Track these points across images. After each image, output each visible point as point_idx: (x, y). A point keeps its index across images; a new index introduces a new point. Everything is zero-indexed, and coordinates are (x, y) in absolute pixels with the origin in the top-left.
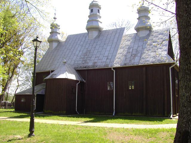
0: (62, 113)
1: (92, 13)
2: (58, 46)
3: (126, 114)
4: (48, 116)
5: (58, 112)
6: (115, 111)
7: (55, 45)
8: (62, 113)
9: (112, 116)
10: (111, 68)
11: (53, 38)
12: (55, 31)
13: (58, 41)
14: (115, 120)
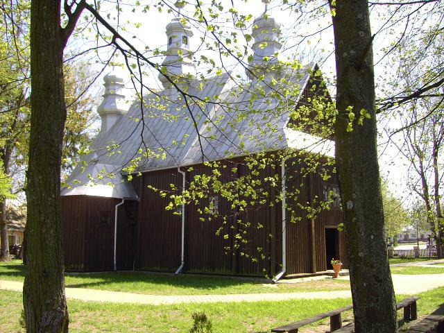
0: (74, 269)
1: (171, 46)
2: (117, 123)
3: (217, 271)
4: (223, 285)
5: (69, 267)
6: (184, 265)
7: (112, 121)
8: (74, 269)
9: (174, 275)
10: (177, 168)
11: (107, 109)
12: (111, 92)
13: (118, 114)
14: (238, 287)
